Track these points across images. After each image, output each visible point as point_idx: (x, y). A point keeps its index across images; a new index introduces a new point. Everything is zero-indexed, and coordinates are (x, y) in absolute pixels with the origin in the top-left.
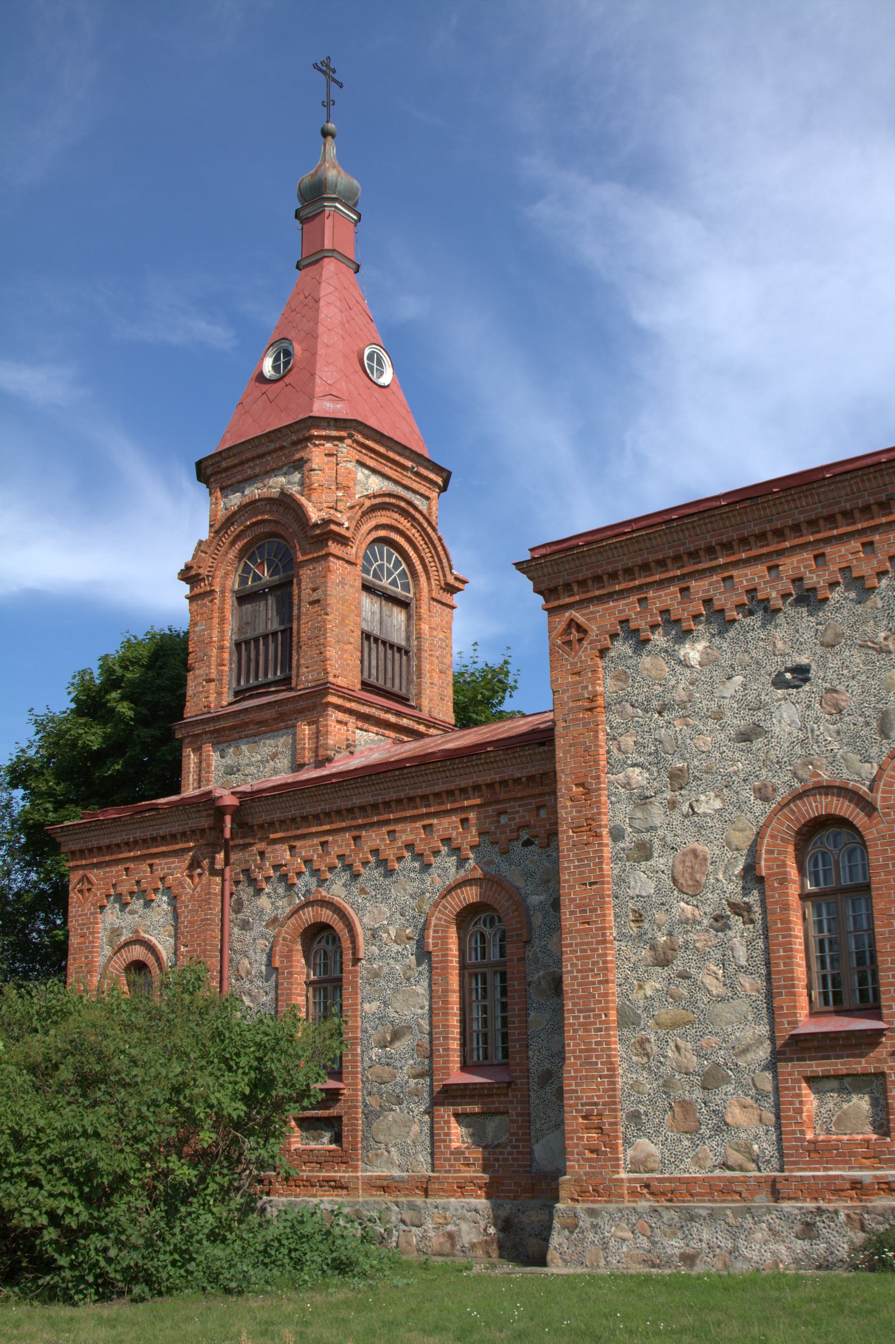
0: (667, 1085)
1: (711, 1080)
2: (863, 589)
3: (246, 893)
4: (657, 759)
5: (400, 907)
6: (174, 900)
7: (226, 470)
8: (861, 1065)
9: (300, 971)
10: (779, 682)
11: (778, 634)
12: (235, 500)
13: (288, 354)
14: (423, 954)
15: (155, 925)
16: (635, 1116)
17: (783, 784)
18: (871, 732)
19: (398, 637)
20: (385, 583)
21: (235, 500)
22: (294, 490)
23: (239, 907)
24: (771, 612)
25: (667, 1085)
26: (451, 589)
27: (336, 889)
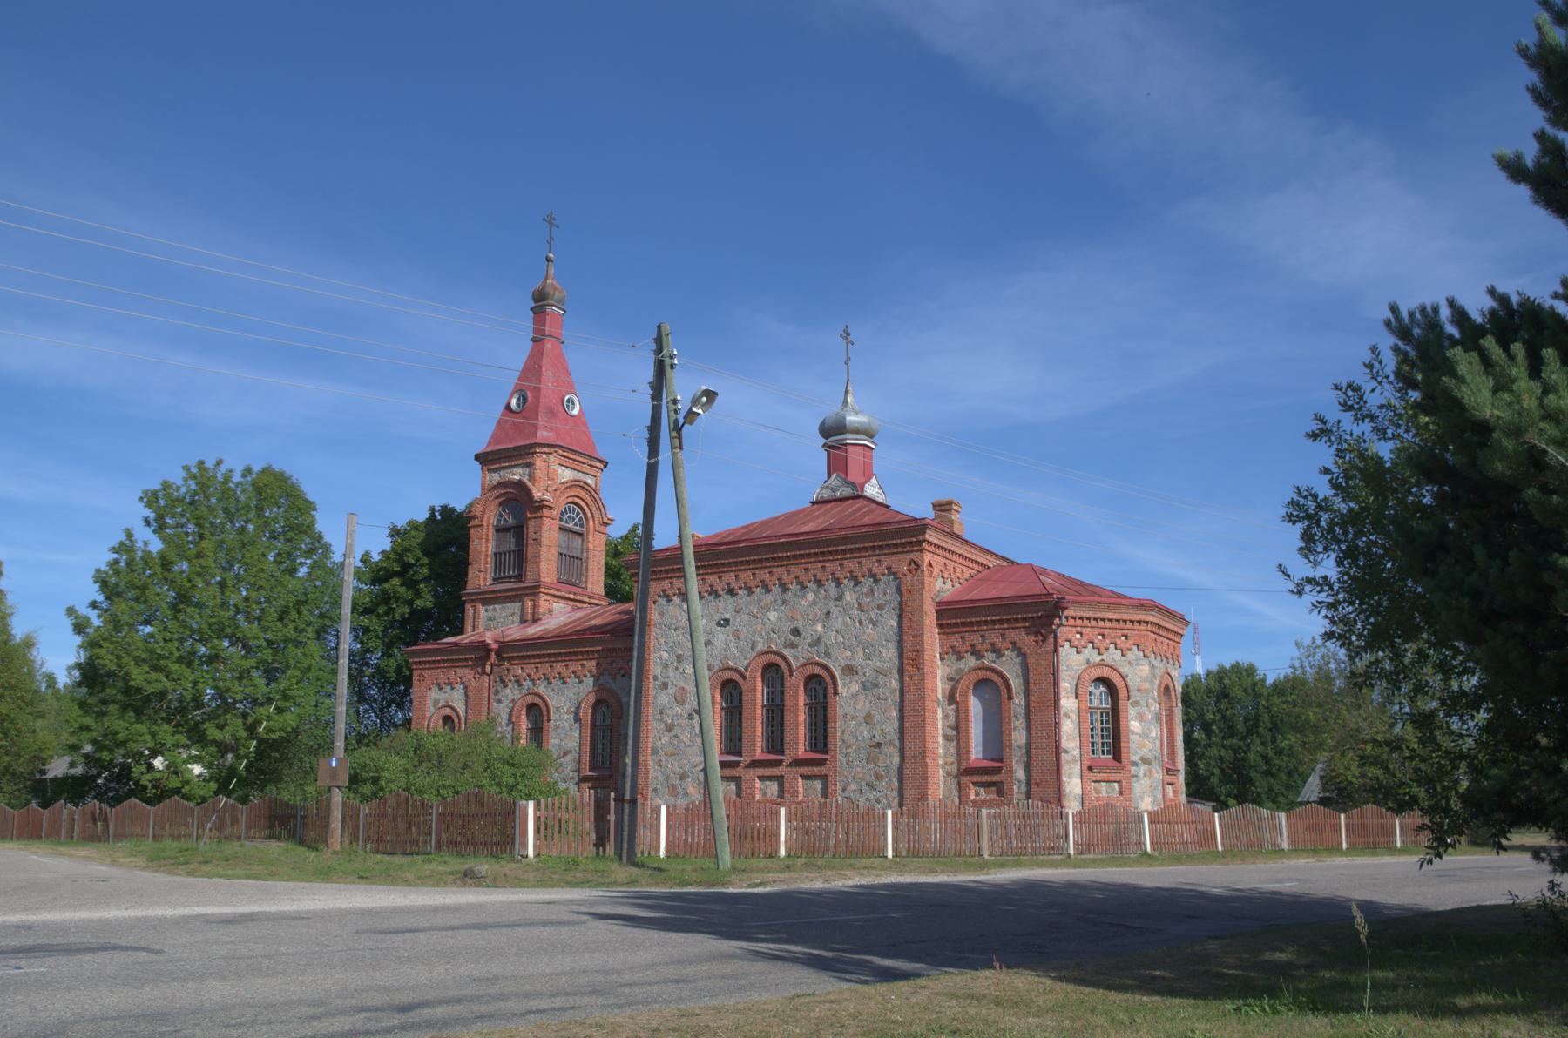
0: (667, 778)
1: (683, 777)
2: (750, 592)
3: (500, 686)
4: (672, 650)
5: (569, 697)
6: (466, 688)
7: (594, 992)
8: (995, 778)
9: (524, 724)
10: (719, 624)
11: (721, 605)
12: (496, 477)
13: (525, 398)
14: (577, 719)
15: (456, 698)
16: (655, 790)
17: (717, 664)
18: (748, 649)
19: (576, 553)
20: (571, 525)
21: (496, 477)
22: (525, 479)
23: (497, 693)
24: (717, 596)
25: (667, 778)
26: (606, 524)
27: (541, 688)
